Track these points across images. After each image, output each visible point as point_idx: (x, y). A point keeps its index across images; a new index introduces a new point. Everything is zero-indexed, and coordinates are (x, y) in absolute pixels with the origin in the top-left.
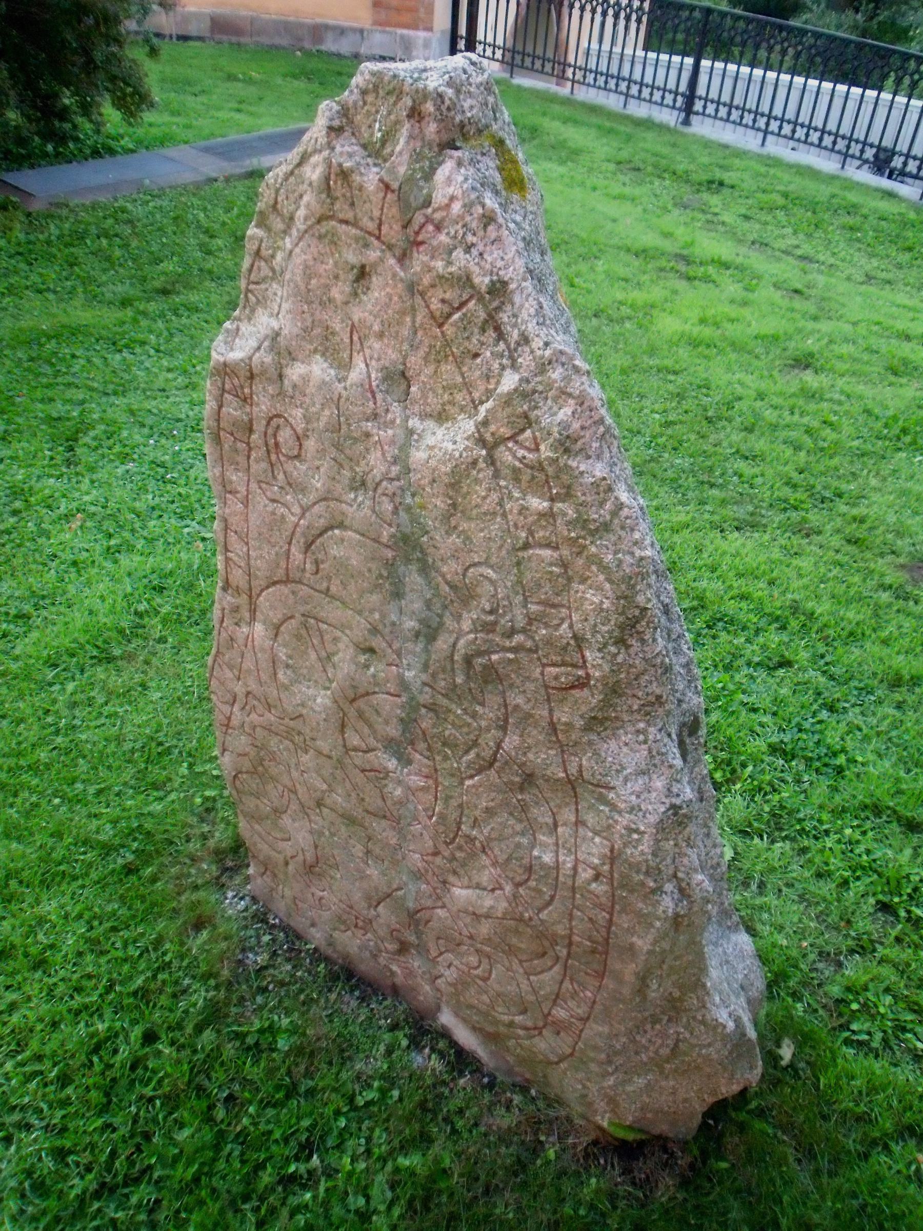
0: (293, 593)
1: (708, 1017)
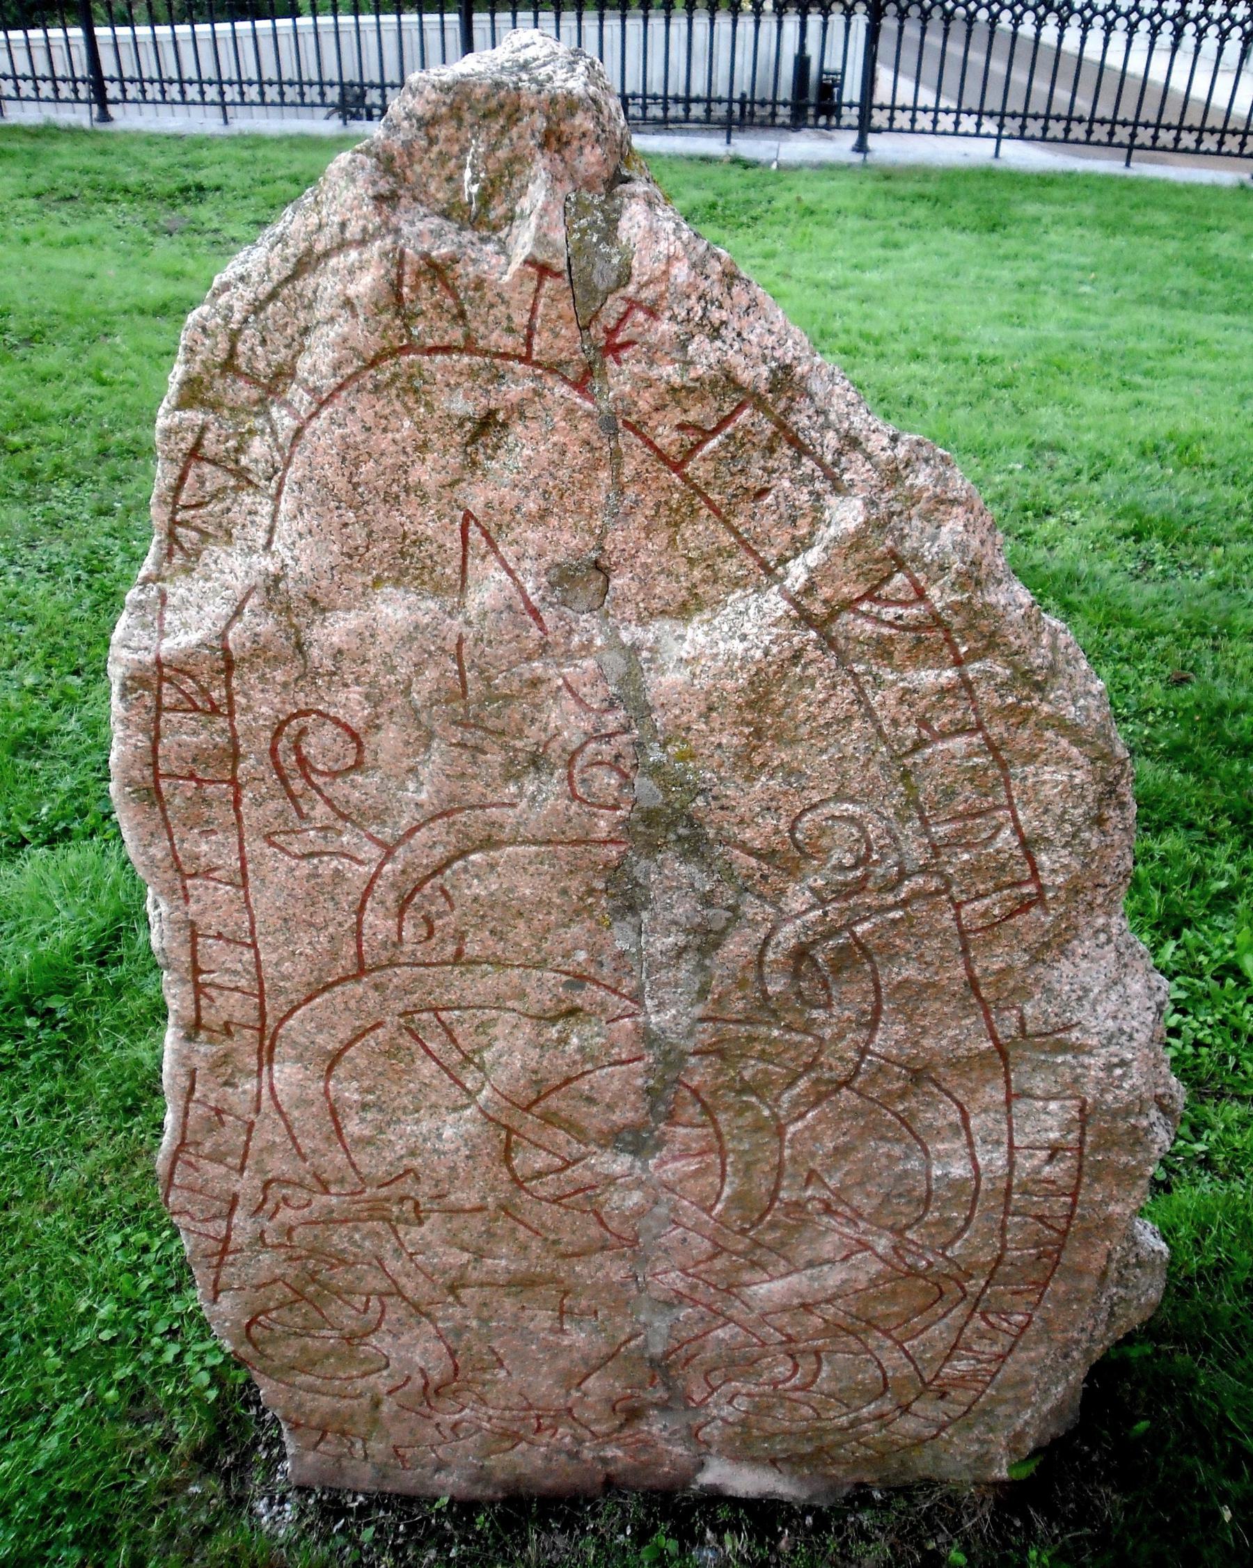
0: (376, 987)
1: (1143, 1253)
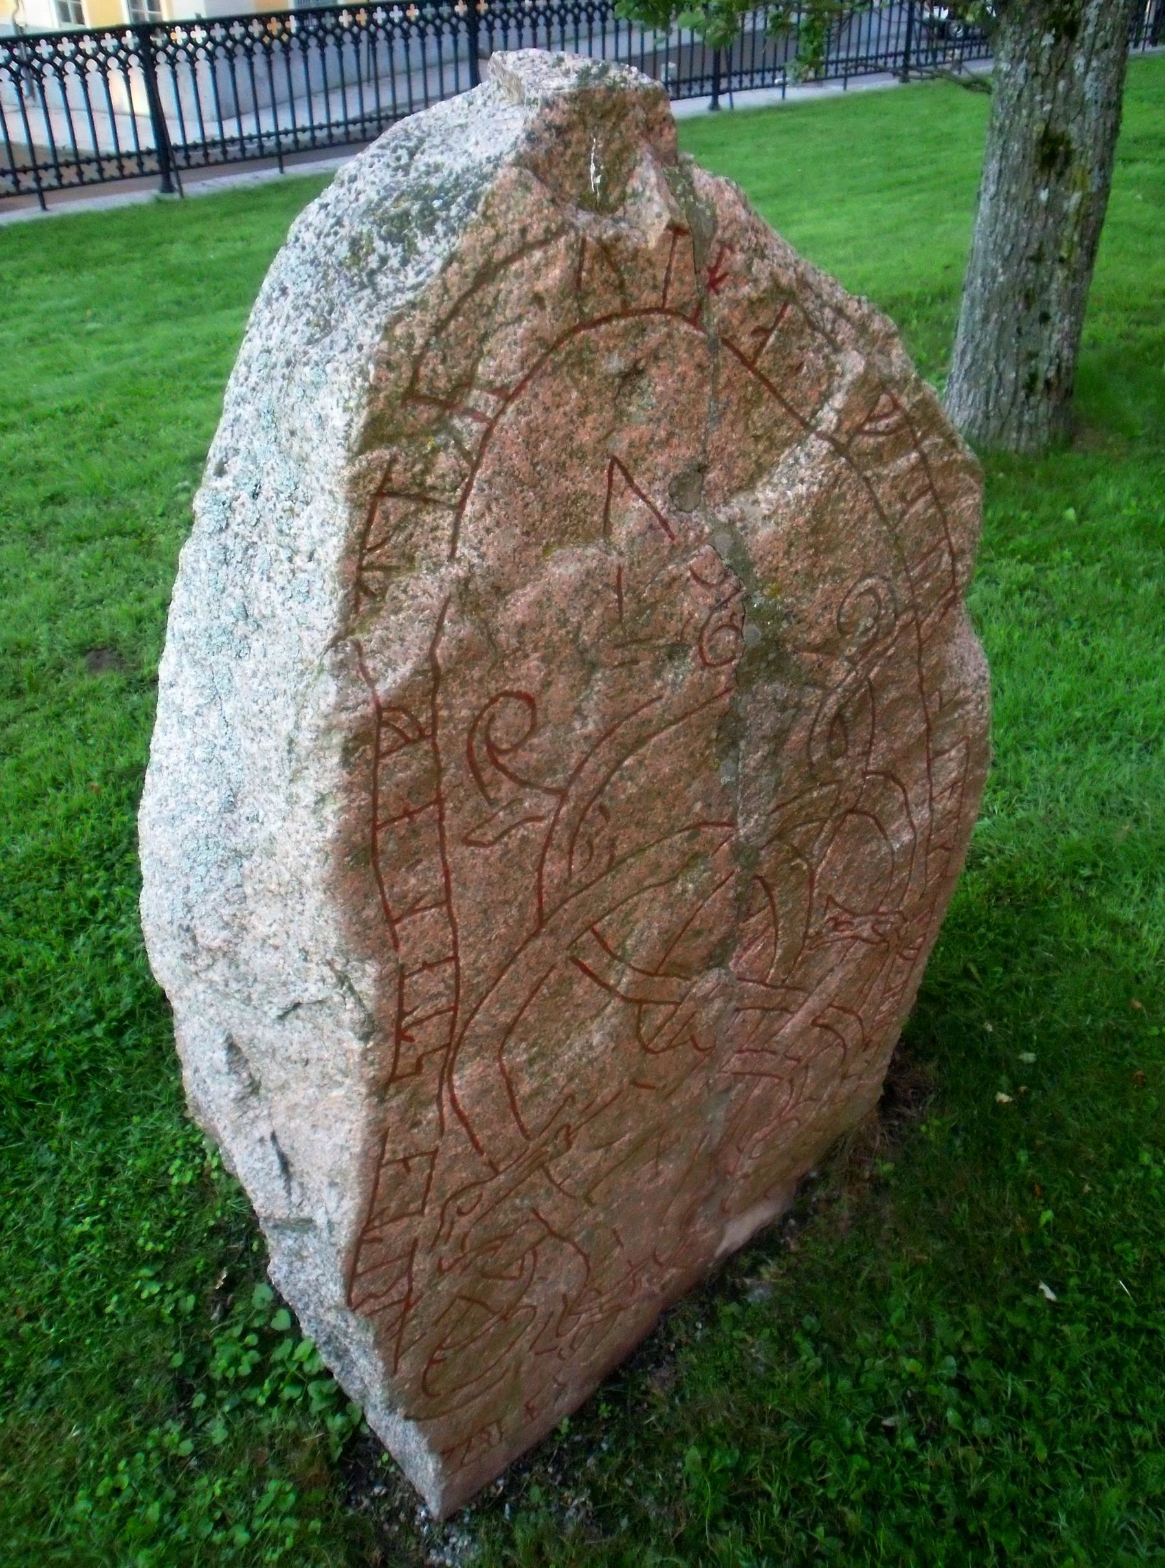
0: (552, 932)
